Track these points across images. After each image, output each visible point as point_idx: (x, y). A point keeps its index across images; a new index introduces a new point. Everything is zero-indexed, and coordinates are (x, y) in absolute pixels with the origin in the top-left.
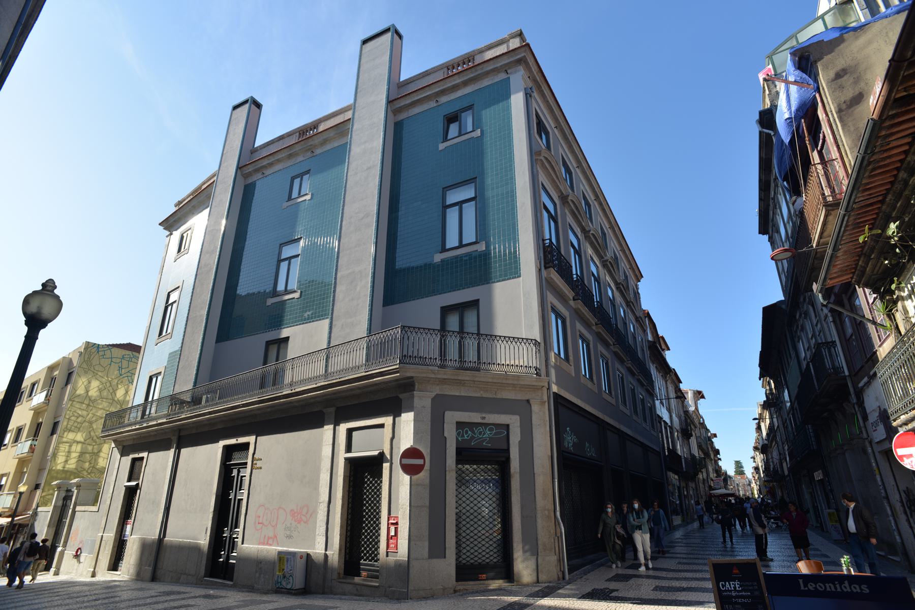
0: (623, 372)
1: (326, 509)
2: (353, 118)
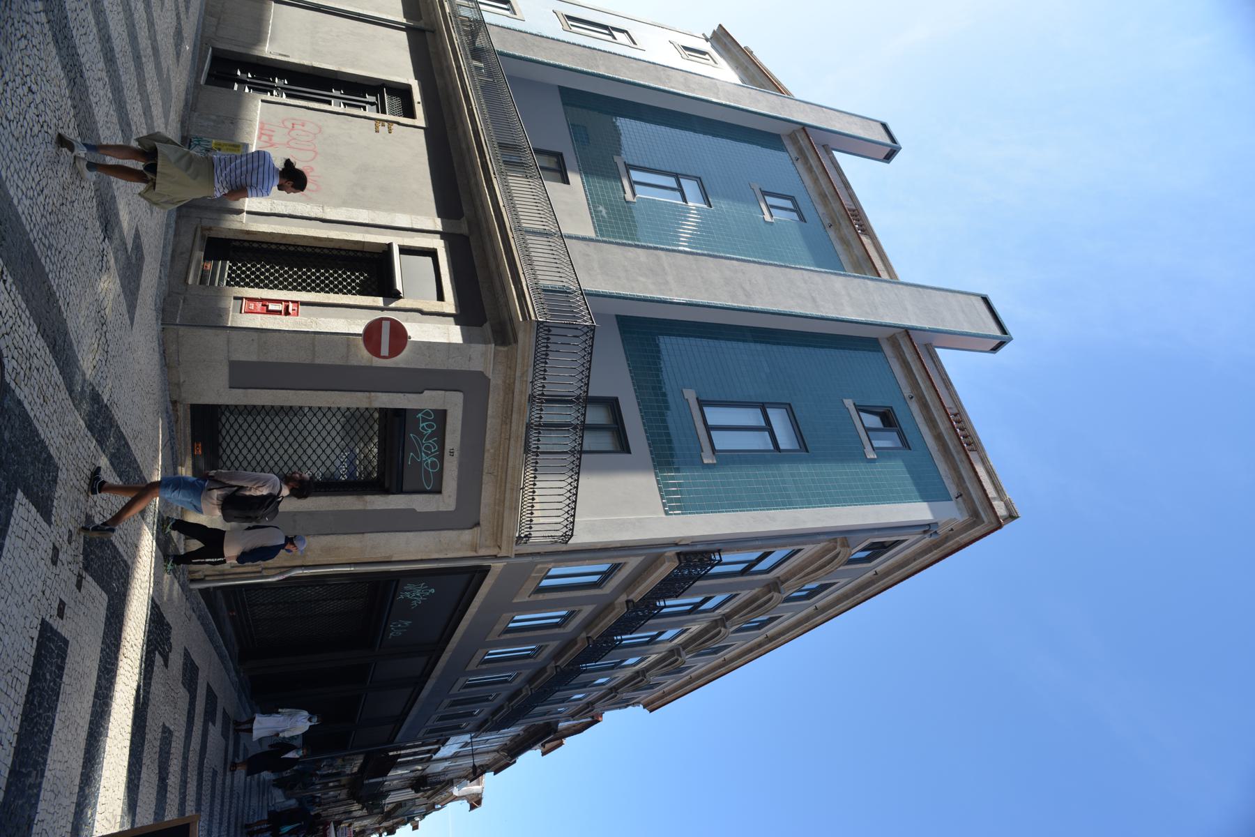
0: (515, 683)
1: (313, 215)
2: (882, 281)
